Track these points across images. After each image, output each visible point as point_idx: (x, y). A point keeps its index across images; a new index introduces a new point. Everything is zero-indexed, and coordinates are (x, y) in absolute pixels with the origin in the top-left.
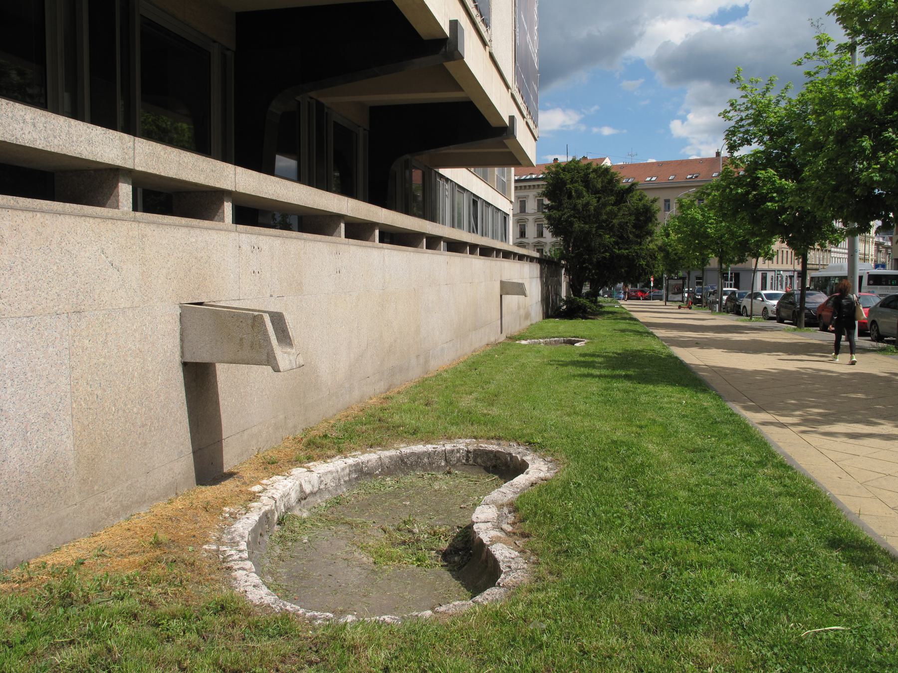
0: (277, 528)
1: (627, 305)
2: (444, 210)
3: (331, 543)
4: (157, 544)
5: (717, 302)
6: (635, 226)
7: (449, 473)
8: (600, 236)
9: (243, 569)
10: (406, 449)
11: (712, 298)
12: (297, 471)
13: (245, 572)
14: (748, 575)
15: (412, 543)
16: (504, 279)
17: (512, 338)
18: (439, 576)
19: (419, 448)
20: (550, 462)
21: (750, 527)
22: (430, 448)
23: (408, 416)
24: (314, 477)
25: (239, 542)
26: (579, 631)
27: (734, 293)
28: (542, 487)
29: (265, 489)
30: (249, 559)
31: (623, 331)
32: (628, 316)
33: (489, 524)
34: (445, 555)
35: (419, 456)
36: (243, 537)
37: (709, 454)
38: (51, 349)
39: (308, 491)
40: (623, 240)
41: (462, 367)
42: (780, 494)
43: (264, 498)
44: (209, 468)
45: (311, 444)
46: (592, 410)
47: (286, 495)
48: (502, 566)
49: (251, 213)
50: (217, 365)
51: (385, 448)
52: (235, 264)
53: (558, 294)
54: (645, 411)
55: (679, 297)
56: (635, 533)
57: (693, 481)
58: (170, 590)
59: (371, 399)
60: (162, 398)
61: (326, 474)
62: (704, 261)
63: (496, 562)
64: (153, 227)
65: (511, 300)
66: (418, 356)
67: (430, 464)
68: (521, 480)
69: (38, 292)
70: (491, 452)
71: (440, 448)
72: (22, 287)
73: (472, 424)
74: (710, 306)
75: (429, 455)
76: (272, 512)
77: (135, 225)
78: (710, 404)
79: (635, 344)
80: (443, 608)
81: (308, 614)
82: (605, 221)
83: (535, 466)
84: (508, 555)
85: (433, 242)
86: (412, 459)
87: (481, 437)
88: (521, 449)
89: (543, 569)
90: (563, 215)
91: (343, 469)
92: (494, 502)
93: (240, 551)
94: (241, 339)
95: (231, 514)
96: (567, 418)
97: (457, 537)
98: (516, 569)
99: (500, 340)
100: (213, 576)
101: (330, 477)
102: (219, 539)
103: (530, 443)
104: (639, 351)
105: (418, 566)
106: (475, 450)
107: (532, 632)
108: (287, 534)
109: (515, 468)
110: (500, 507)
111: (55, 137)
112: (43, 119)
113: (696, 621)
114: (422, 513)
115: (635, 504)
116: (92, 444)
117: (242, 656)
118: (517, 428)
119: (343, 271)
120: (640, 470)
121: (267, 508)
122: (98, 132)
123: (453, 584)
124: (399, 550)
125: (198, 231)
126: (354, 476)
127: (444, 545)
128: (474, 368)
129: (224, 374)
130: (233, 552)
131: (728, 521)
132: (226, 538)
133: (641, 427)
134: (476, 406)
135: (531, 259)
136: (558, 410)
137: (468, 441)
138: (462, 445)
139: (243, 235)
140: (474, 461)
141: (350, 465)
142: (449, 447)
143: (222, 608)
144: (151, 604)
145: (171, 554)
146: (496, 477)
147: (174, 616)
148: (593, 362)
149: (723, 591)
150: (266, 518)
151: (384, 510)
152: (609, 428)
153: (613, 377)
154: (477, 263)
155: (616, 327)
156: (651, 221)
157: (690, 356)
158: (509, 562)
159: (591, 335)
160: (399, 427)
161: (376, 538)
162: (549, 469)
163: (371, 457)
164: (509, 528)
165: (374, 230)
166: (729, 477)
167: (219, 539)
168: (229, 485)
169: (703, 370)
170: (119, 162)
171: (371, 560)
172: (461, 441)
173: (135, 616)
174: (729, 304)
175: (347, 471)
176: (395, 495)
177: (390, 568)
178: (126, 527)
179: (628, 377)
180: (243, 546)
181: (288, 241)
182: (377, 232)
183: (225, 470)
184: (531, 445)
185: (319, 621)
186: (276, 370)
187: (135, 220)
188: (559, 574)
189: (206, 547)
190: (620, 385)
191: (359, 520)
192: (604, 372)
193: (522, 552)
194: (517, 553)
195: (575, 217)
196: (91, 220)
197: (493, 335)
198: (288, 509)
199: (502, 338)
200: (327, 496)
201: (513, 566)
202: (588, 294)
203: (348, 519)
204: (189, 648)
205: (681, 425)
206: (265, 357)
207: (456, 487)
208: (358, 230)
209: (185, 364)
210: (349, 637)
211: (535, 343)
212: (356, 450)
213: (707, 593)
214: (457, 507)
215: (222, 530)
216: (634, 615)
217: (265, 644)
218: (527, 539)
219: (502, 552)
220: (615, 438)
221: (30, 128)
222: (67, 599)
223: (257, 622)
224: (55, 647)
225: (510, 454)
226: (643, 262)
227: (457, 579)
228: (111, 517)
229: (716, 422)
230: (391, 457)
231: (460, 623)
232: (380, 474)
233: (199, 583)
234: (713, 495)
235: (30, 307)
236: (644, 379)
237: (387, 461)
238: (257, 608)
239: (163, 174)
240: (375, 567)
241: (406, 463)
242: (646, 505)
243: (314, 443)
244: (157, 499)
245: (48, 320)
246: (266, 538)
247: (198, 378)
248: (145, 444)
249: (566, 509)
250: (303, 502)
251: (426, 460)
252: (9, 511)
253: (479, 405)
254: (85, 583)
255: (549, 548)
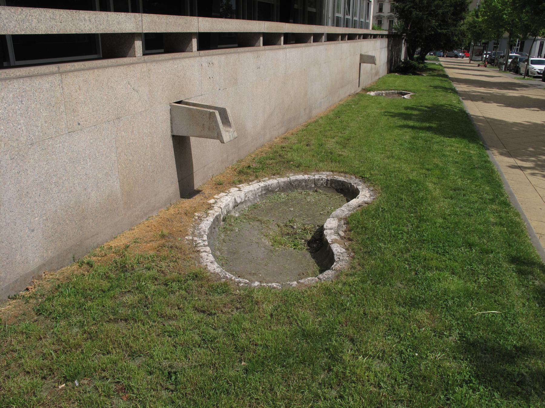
0: (222, 223)
1: (443, 61)
2: (328, 11)
3: (250, 232)
4: (163, 236)
5: (504, 64)
6: (453, 14)
7: (316, 191)
8: (429, 21)
9: (205, 252)
10: (293, 178)
11: (501, 60)
12: (233, 190)
13: (206, 254)
14: (460, 277)
15: (293, 235)
16: (363, 53)
17: (366, 90)
18: (304, 256)
19: (300, 177)
20: (372, 191)
21: (470, 246)
22: (306, 177)
23: (296, 154)
24: (242, 194)
25: (203, 235)
26: (365, 302)
27: (516, 57)
28: (364, 209)
29: (216, 202)
30: (208, 245)
31: (436, 87)
32: (441, 73)
33: (333, 231)
34: (309, 243)
35: (300, 181)
36: (205, 232)
37: (462, 192)
38: (106, 140)
39: (239, 202)
40: (444, 23)
41: (331, 115)
42: (496, 224)
43: (216, 208)
44: (187, 190)
45: (240, 172)
46: (402, 156)
47: (227, 205)
48: (336, 258)
49: (209, 42)
50: (191, 138)
51: (281, 176)
52: (200, 75)
53: (399, 56)
54: (434, 157)
55: (479, 58)
56: (407, 245)
57: (447, 212)
58: (172, 264)
59: (276, 138)
60: (162, 156)
61: (248, 192)
62: (499, 36)
63: (333, 254)
64: (154, 64)
65: (366, 67)
66: (305, 109)
67: (306, 186)
68: (354, 202)
69: (99, 112)
70: (340, 181)
71: (312, 177)
72: (91, 111)
73: (332, 162)
74: (499, 65)
75: (305, 181)
76: (220, 215)
77: (144, 65)
78: (475, 152)
79: (443, 99)
80: (302, 281)
81: (237, 280)
82: (434, 11)
83: (363, 193)
84: (339, 251)
85: (317, 37)
86: (296, 183)
87: (336, 171)
88: (357, 181)
89: (356, 261)
90: (406, 6)
91: (258, 189)
92: (337, 216)
93: (204, 241)
94: (203, 125)
95: (199, 217)
96: (387, 161)
97: (316, 232)
98: (342, 260)
99: (358, 92)
100: (191, 255)
101: (251, 193)
102: (193, 233)
103: (362, 177)
104: (442, 105)
105: (294, 249)
106: (331, 180)
107: (342, 300)
108: (227, 227)
109: (352, 193)
110: (340, 219)
111: (101, 25)
112: (94, 16)
113: (424, 302)
114: (299, 216)
115: (412, 225)
116: (128, 184)
117: (206, 304)
118: (356, 166)
119: (261, 67)
120: (419, 202)
121: (217, 214)
122: (123, 16)
123: (311, 261)
124: (285, 238)
125: (178, 61)
126: (264, 192)
127: (309, 237)
128: (338, 115)
129: (194, 142)
130: (200, 241)
131: (460, 241)
132: (197, 232)
133: (428, 170)
134: (336, 148)
135: (382, 36)
136: (382, 153)
137: (328, 173)
138: (324, 176)
139: (203, 58)
140: (331, 185)
141: (262, 187)
142: (317, 177)
143: (195, 276)
144: (163, 272)
145: (171, 242)
146: (342, 195)
147: (174, 281)
148: (411, 114)
149: (444, 285)
150: (217, 219)
151: (279, 213)
152: (409, 170)
153: (421, 128)
154: (345, 46)
155: (432, 84)
156: (464, 10)
157: (474, 109)
158: (339, 255)
159: (416, 90)
160: (290, 161)
161: (274, 231)
162: (371, 196)
163: (273, 182)
164: (342, 234)
165: (281, 37)
166: (470, 210)
167: (193, 233)
168: (197, 199)
169: (481, 121)
170: (134, 31)
171: (270, 243)
172: (324, 173)
173: (156, 279)
174: (512, 65)
175: (260, 190)
176: (285, 203)
177: (279, 249)
178: (147, 225)
179: (429, 129)
180: (205, 238)
181: (229, 56)
182: (282, 38)
183: (196, 188)
184: (363, 179)
185: (242, 284)
186: (222, 142)
187: (145, 62)
188: (363, 266)
189: (186, 237)
190: (423, 135)
191: (265, 219)
192: (417, 124)
193: (347, 249)
194: (344, 250)
195: (414, 8)
196: (122, 68)
197: (354, 89)
198: (228, 212)
199: (359, 90)
200: (249, 204)
201: (341, 258)
202: (417, 58)
203: (260, 218)
204: (182, 298)
205: (452, 169)
206: (216, 135)
207: (319, 200)
208: (270, 39)
209: (173, 136)
210: (255, 296)
211: (380, 93)
212: (265, 177)
213: (436, 285)
214: (318, 213)
215: (194, 227)
216: (394, 295)
217: (217, 297)
218: (350, 242)
219: (337, 249)
220: (411, 178)
221: (88, 23)
222: (123, 268)
223: (213, 285)
224: (123, 294)
225: (350, 184)
226: (455, 38)
227: (314, 258)
228: (139, 219)
229: (474, 168)
230: (284, 182)
231: (309, 292)
232: (278, 191)
233: (184, 259)
234: (456, 223)
235: (95, 120)
236: (439, 131)
237: (282, 184)
238: (212, 275)
239: (158, 32)
240: (272, 248)
241: (292, 185)
242: (418, 227)
243: (243, 172)
244: (161, 207)
245: (104, 125)
246: (217, 229)
247: (181, 144)
248: (154, 181)
249: (374, 225)
250: (236, 208)
251: (304, 184)
252: (93, 222)
253: (338, 147)
254: (131, 261)
255: (361, 250)
